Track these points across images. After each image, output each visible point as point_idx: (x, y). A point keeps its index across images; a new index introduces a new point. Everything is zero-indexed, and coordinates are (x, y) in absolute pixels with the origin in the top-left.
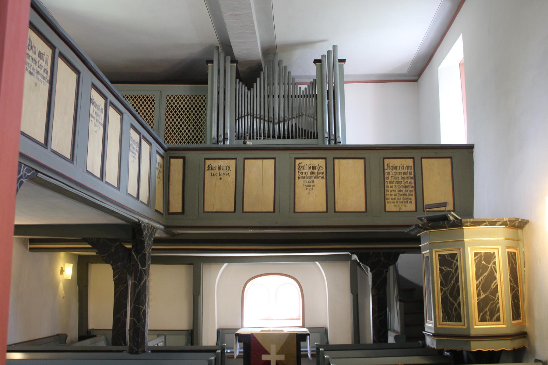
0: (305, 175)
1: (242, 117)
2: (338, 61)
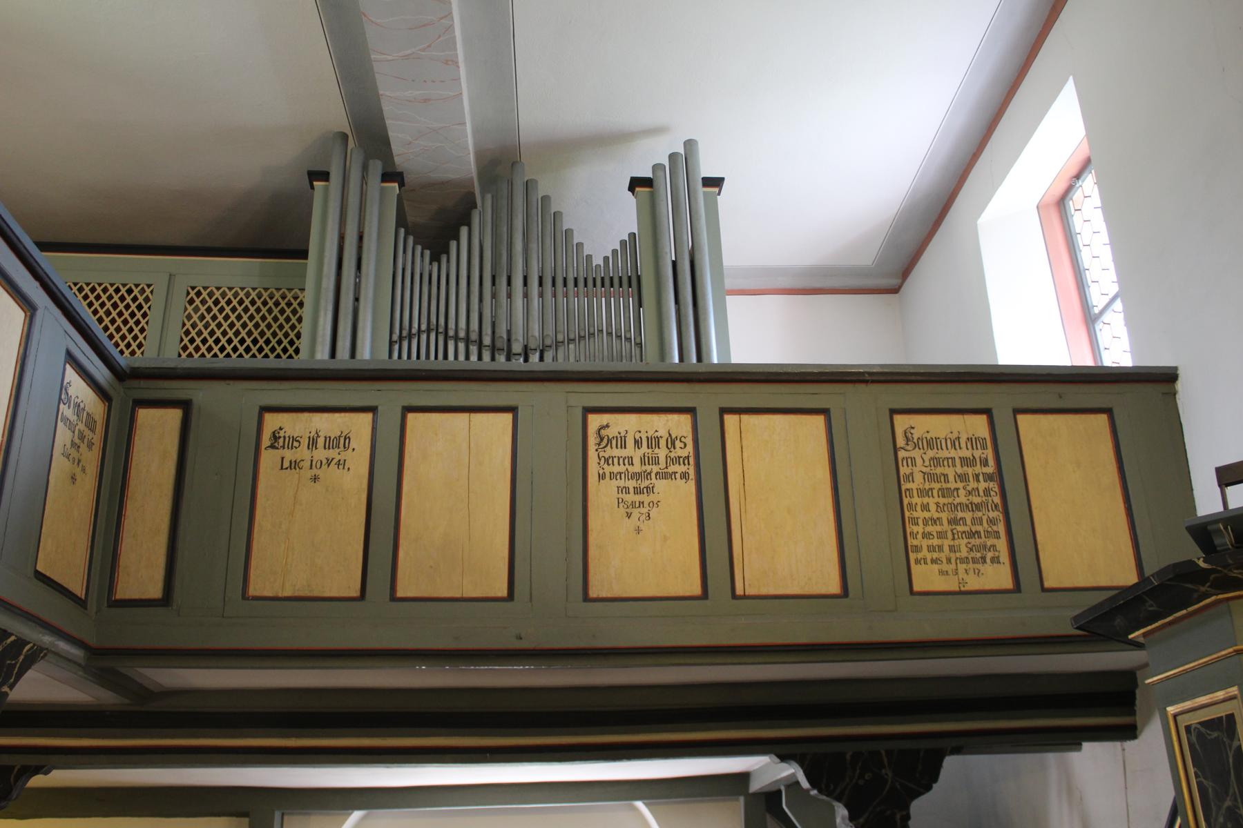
0: (622, 468)
1: (410, 336)
2: (700, 182)
